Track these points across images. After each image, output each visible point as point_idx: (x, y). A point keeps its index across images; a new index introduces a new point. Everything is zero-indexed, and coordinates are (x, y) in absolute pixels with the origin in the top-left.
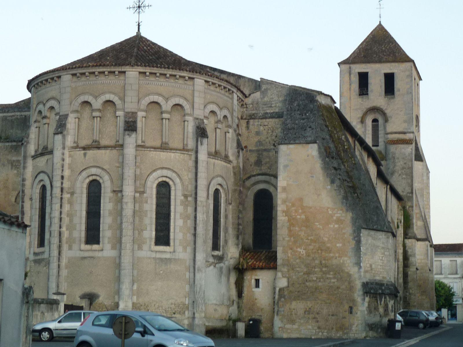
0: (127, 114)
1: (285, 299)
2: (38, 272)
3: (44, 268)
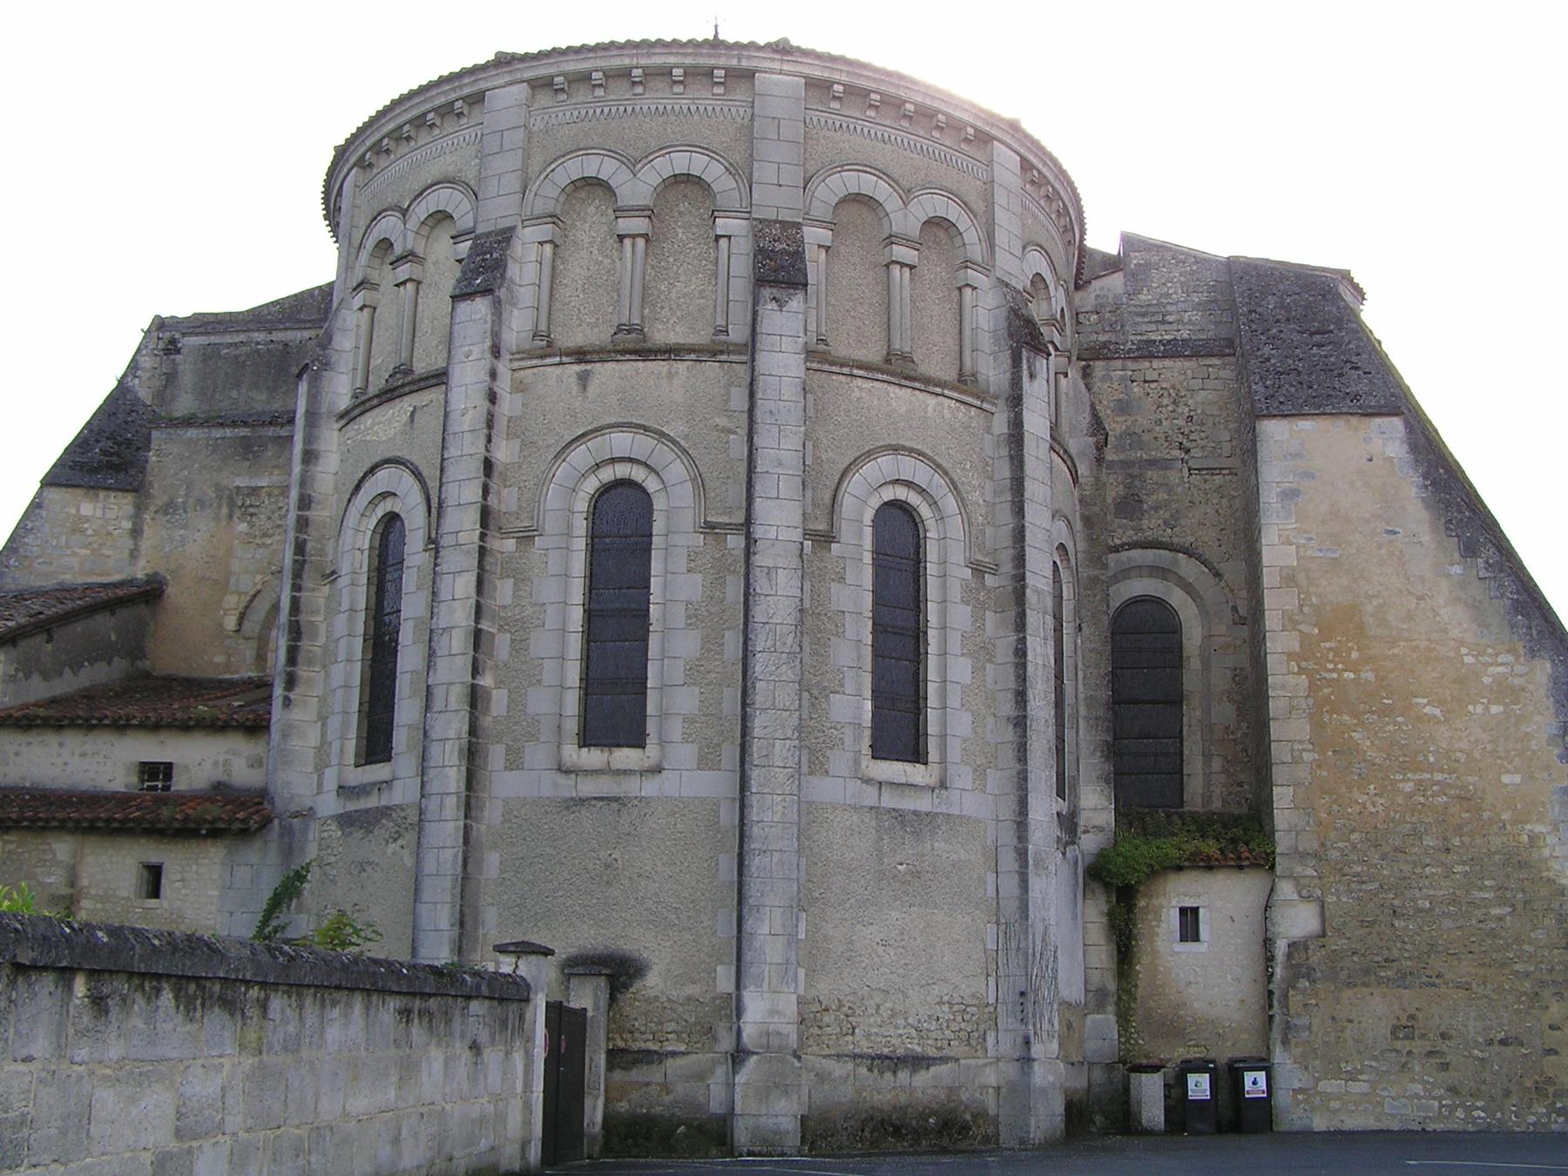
0: (760, 228)
1: (1313, 982)
2: (362, 865)
3: (392, 847)
